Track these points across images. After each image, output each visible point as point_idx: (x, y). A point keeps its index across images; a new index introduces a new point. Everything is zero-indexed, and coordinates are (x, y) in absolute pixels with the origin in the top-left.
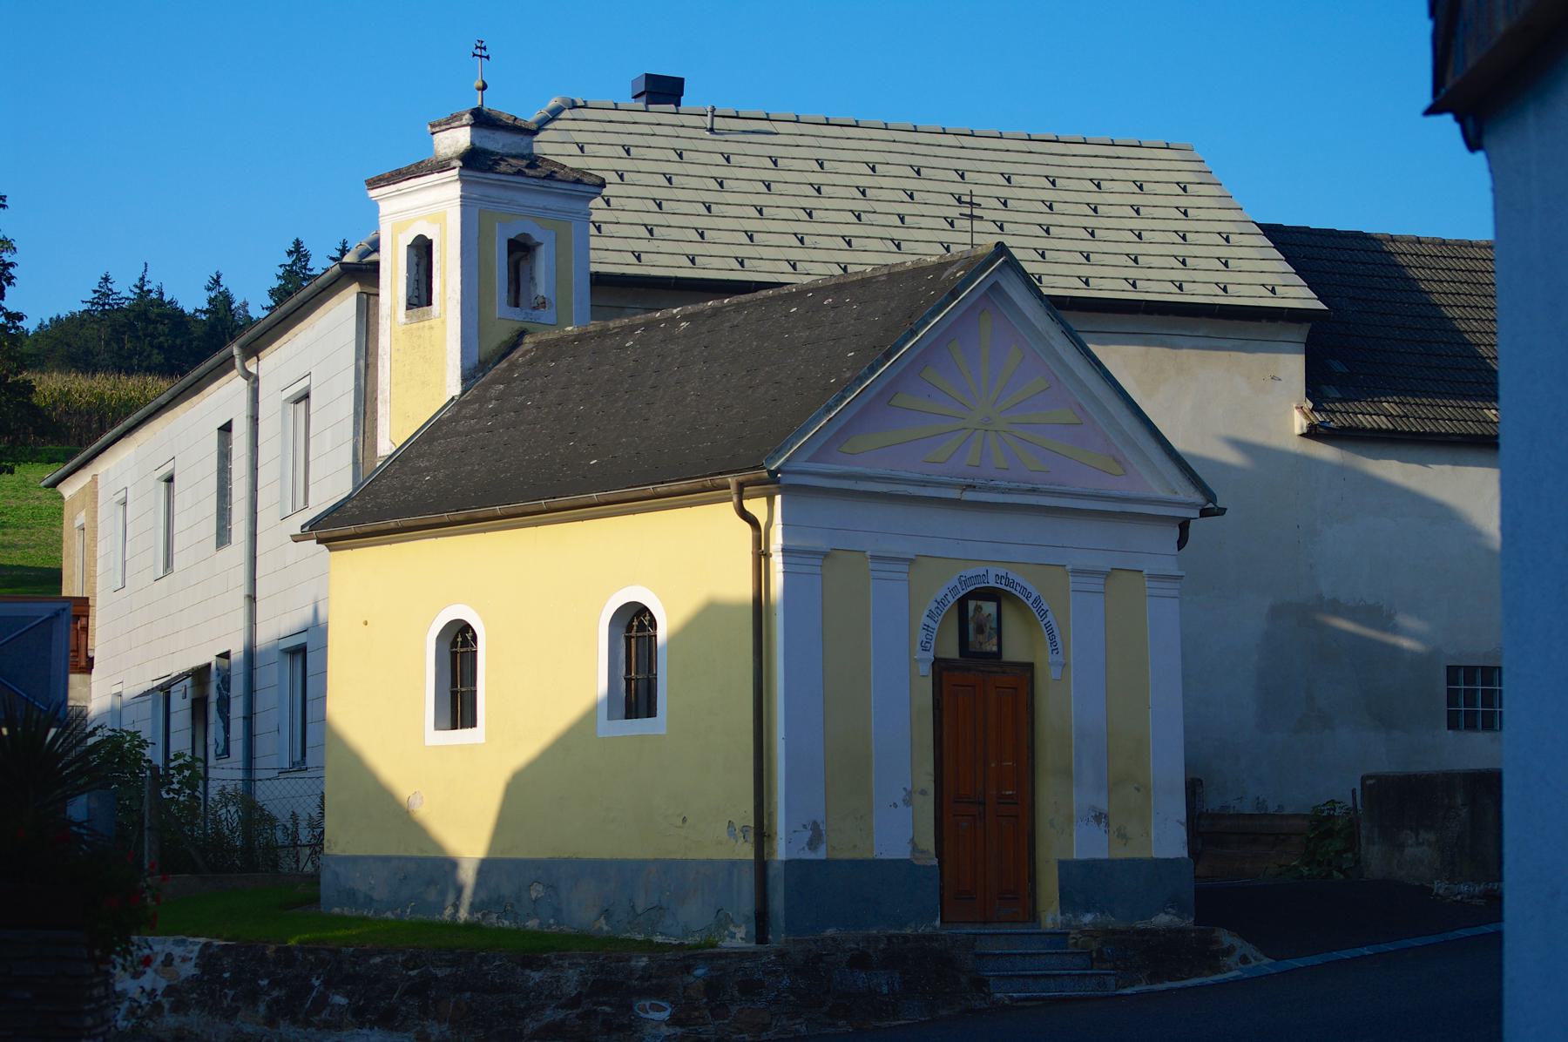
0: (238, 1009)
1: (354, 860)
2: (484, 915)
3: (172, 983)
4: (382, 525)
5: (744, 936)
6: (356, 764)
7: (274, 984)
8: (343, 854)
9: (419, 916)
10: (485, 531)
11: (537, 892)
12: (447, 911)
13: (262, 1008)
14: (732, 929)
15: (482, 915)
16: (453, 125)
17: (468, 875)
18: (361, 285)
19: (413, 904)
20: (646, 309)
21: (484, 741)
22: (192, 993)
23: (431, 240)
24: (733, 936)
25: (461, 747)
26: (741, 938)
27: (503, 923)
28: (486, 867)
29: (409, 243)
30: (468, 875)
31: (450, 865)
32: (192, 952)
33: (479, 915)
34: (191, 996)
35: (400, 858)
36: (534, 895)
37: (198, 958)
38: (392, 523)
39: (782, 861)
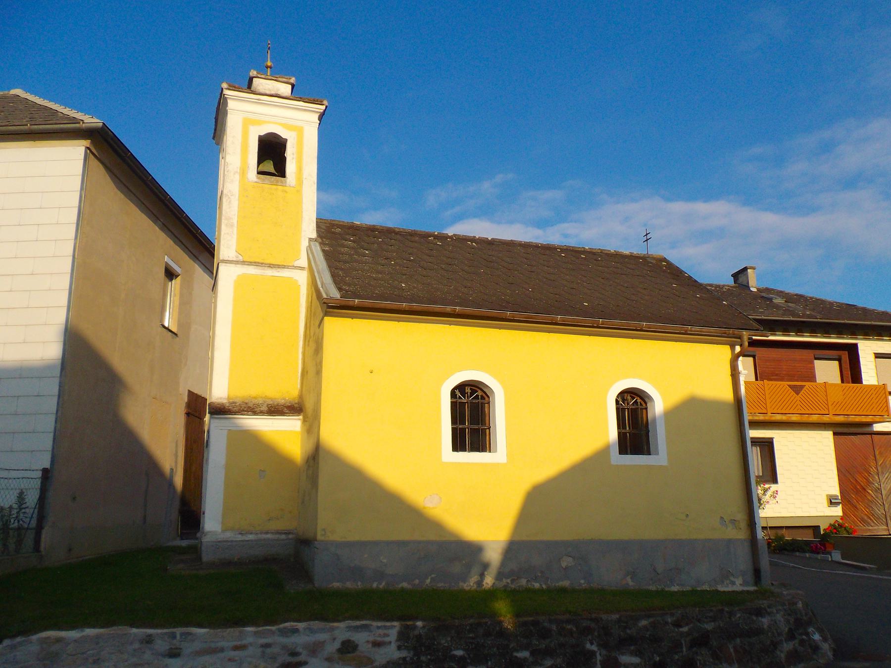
1: (363, 544)
2: (513, 581)
4: (437, 307)
5: (741, 583)
8: (343, 540)
9: (440, 585)
10: (590, 335)
11: (566, 562)
14: (732, 579)
15: (511, 581)
17: (494, 556)
18: (92, 143)
19: (433, 576)
20: (163, 224)
21: (505, 461)
23: (286, 140)
24: (733, 583)
26: (741, 585)
27: (534, 586)
28: (513, 548)
30: (494, 556)
32: (387, 635)
33: (509, 581)
36: (564, 565)
37: (397, 641)
39: (316, 537)
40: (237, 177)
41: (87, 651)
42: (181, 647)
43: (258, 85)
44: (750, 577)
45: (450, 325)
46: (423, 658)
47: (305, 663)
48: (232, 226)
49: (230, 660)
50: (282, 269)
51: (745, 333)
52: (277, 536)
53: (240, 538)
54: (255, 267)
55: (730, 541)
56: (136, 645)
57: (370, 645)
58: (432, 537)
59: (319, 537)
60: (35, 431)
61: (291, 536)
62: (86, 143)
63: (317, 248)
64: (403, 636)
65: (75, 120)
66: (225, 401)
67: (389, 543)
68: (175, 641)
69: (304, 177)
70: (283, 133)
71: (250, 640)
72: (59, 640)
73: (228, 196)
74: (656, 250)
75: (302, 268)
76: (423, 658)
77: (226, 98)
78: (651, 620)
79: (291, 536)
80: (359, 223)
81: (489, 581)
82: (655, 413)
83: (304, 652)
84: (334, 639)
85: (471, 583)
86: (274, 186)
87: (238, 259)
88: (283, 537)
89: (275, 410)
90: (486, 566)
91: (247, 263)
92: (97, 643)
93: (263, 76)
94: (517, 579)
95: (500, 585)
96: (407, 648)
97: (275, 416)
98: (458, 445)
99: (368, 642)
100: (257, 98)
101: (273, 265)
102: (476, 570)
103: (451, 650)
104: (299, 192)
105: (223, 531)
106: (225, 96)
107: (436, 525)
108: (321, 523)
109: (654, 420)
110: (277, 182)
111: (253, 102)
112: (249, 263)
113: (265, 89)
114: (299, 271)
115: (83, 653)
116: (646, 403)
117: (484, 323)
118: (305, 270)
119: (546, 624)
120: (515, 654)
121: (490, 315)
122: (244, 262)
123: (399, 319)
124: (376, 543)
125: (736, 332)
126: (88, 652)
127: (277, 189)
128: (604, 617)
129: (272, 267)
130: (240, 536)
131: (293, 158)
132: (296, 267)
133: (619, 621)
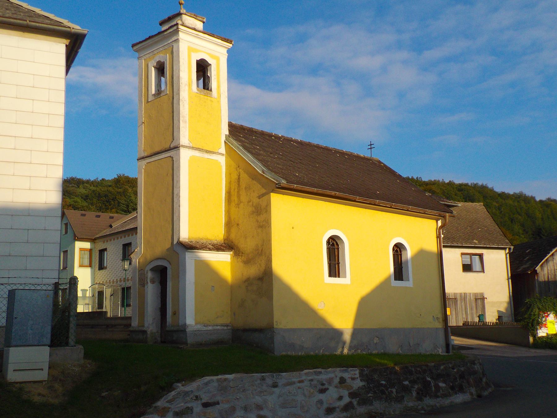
0: (403, 397)
1: (294, 330)
3: (350, 391)
4: (328, 192)
6: (288, 290)
7: (413, 382)
8: (285, 328)
10: (346, 205)
11: (376, 340)
12: (339, 350)
13: (414, 394)
16: (198, 18)
17: (347, 337)
22: (368, 394)
25: (341, 285)
28: (356, 332)
29: (198, 59)
30: (347, 337)
31: (337, 334)
32: (355, 374)
34: (369, 395)
35: (317, 329)
36: (375, 342)
38: (333, 193)
40: (187, 88)
41: (239, 385)
42: (277, 382)
43: (185, 20)
44: (444, 349)
45: (325, 201)
46: (371, 385)
47: (328, 389)
48: (186, 122)
49: (299, 388)
50: (213, 154)
51: (447, 214)
52: (223, 327)
53: (205, 328)
54: (199, 151)
55: (437, 328)
56: (259, 382)
57: (350, 379)
58: (322, 326)
59: (275, 326)
60: (11, 255)
61: (229, 328)
62: (67, 42)
63: (235, 144)
64: (361, 375)
65: (60, 24)
66: (187, 241)
67: (305, 330)
68: (274, 379)
69: (221, 92)
70: (210, 61)
71: (304, 378)
72: (226, 380)
73: (183, 101)
74: (376, 155)
75: (223, 155)
76: (371, 385)
77: (179, 30)
78: (444, 366)
79: (229, 328)
80: (234, 123)
81: (346, 351)
82: (408, 258)
83: (326, 384)
84: (336, 376)
85: (338, 352)
86: (206, 97)
87: (190, 145)
88: (225, 328)
89: (218, 248)
90: (344, 343)
91: (195, 149)
92: (242, 381)
93: (189, 14)
94: (357, 350)
95: (350, 353)
96: (364, 381)
97: (219, 251)
98: (330, 275)
99: (349, 377)
100: (197, 34)
101: (208, 151)
102: (340, 345)
103: (380, 382)
104: (219, 102)
105: (196, 324)
106: (179, 29)
107: (322, 320)
108: (276, 318)
109: (407, 262)
110: (208, 94)
111: (214, 43)
112: (196, 149)
113: (189, 24)
114: (221, 156)
115: (237, 387)
116: (401, 251)
117: (330, 200)
118: (224, 156)
119: (410, 368)
120: (404, 383)
121: (303, 189)
122: (193, 147)
123: (303, 196)
124: (300, 329)
125: (442, 213)
126: (239, 386)
127: (207, 99)
128: (429, 364)
129: (207, 152)
130: (205, 327)
131: (215, 78)
132: (219, 153)
133: (435, 366)
